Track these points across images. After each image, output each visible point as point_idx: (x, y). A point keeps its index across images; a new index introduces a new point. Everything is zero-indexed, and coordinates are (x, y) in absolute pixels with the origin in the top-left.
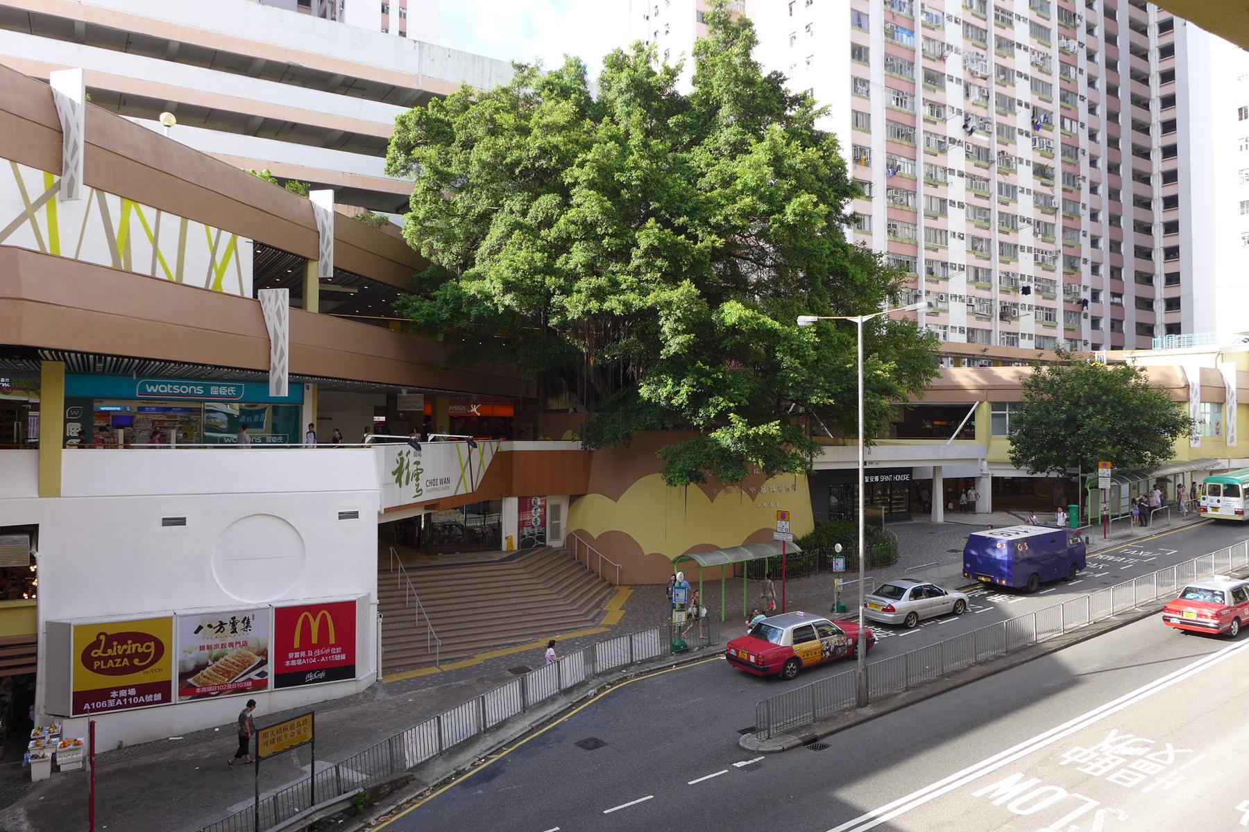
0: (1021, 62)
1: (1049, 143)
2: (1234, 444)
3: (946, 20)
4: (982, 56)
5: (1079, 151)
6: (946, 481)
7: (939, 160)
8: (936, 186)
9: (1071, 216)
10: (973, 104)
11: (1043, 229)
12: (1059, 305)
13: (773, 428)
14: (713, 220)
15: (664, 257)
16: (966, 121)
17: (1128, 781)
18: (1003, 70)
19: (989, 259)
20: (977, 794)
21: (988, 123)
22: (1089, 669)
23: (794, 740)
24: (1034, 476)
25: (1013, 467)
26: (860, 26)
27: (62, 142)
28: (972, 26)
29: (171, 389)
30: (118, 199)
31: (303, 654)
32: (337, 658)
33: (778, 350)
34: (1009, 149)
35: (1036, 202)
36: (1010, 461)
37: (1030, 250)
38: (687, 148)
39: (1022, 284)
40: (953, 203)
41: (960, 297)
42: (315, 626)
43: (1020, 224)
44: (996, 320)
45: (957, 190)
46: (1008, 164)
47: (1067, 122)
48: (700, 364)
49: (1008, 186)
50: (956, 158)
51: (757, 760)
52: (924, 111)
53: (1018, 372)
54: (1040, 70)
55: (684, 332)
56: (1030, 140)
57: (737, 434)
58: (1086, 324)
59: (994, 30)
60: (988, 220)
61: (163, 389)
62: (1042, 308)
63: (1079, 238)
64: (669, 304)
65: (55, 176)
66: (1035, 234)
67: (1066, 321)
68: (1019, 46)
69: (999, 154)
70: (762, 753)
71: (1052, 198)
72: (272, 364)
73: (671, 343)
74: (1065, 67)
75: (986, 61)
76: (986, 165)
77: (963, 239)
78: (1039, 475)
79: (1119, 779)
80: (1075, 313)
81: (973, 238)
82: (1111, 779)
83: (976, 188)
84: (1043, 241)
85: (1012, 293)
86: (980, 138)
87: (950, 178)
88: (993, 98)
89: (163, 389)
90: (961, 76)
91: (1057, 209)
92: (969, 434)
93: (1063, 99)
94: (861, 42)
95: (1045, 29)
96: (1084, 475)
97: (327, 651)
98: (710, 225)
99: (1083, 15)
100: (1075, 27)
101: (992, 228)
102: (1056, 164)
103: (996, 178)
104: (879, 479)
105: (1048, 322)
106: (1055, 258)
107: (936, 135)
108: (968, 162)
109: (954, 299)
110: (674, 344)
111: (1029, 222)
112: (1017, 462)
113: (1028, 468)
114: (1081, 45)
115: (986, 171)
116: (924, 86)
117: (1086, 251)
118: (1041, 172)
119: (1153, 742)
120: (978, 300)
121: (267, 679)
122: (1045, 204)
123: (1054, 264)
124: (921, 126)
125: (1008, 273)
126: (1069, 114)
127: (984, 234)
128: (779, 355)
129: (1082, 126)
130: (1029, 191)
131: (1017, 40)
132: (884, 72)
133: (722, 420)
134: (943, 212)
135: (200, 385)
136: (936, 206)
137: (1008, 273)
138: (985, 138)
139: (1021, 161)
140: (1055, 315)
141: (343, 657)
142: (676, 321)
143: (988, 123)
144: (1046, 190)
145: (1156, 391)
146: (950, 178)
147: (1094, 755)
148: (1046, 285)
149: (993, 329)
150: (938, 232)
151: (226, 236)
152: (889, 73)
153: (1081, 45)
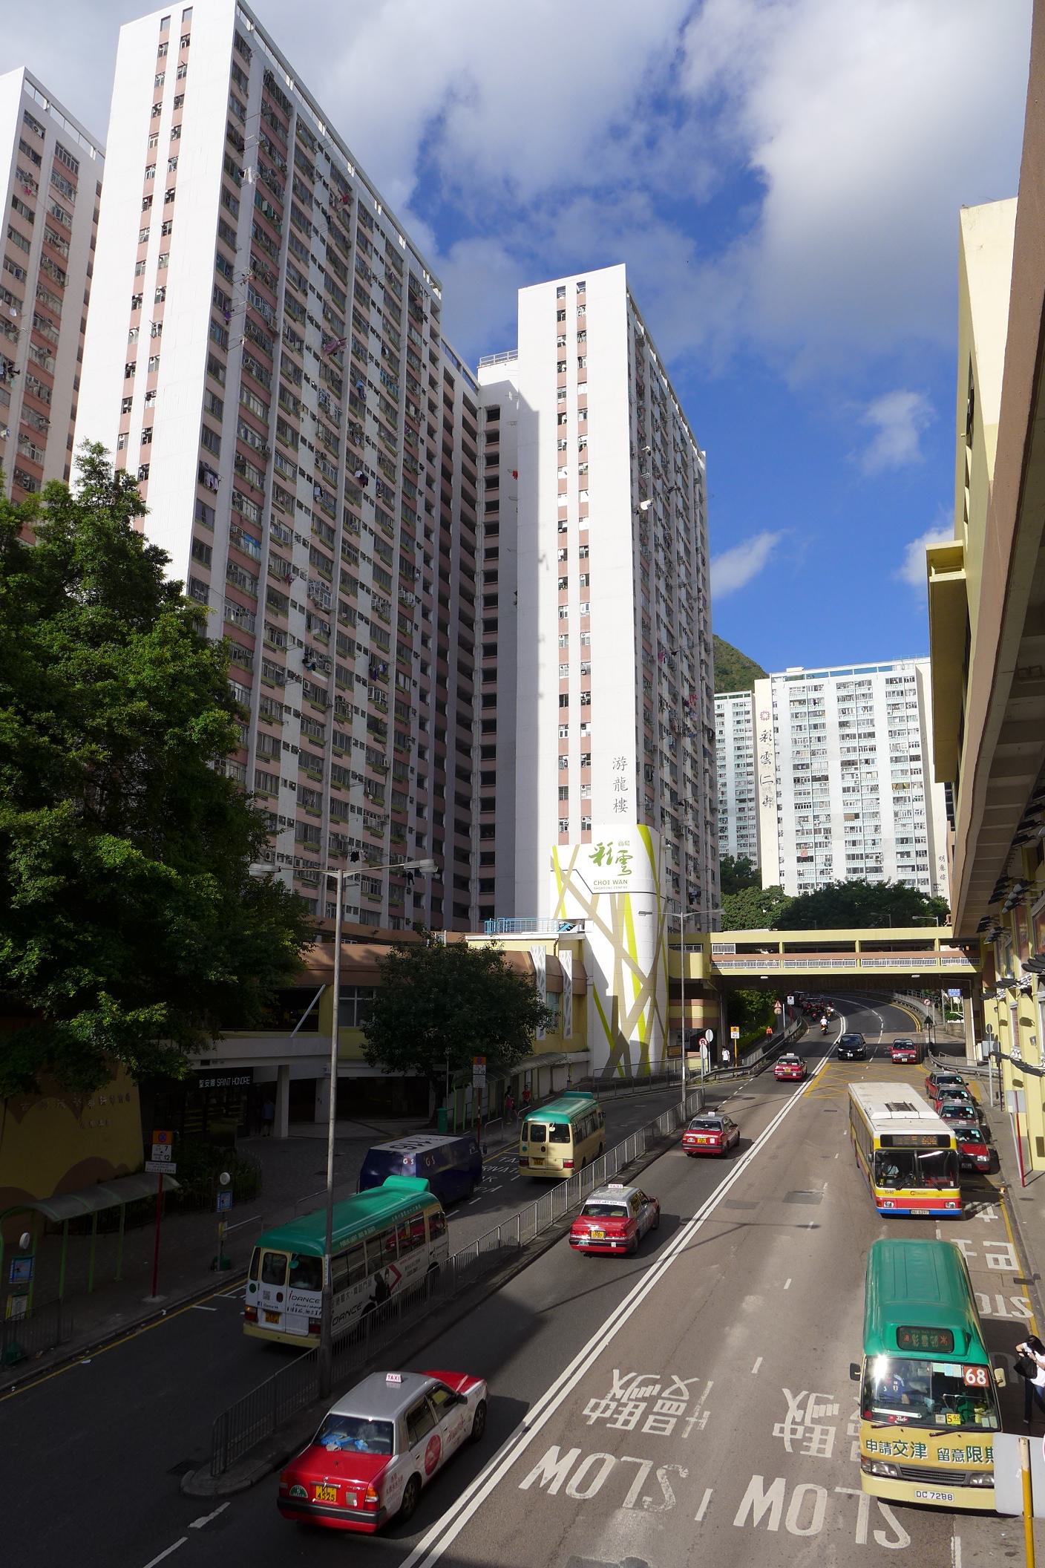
0: (363, 603)
1: (384, 696)
2: (571, 1036)
3: (294, 540)
4: (328, 588)
5: (411, 710)
6: (292, 1083)
7: (274, 694)
8: (270, 724)
9: (400, 779)
10: (315, 638)
11: (373, 790)
12: (385, 877)
13: (158, 1012)
14: (90, 723)
15: (15, 764)
16: (306, 655)
17: (664, 1429)
18: (345, 608)
19: (319, 816)
20: (525, 1485)
21: (328, 662)
22: (549, 1300)
23: (261, 1466)
24: (390, 1075)
25: (367, 1065)
26: (204, 520)
28: (319, 553)
33: (168, 907)
34: (346, 695)
35: (368, 758)
36: (364, 1058)
37: (360, 810)
38: (33, 620)
39: (352, 848)
40: (286, 746)
41: (288, 857)
43: (352, 781)
44: (323, 889)
45: (291, 732)
46: (344, 711)
47: (401, 677)
48: (59, 918)
49: (342, 735)
50: (293, 695)
51: (221, 1509)
52: (263, 635)
53: (368, 952)
54: (380, 617)
55: (48, 873)
56: (366, 689)
57: (107, 1021)
58: (409, 900)
59: (340, 564)
60: (320, 772)
62: (368, 878)
63: (406, 804)
64: (28, 830)
66: (366, 794)
67: (391, 895)
68: (363, 586)
69: (336, 697)
70: (224, 1497)
71: (384, 756)
73: (29, 885)
74: (403, 619)
75: (330, 594)
76: (323, 708)
77: (294, 789)
78: (396, 1074)
79: (652, 1428)
80: (399, 887)
81: (305, 788)
82: (646, 1429)
83: (311, 732)
84: (373, 802)
85: (340, 858)
86: (318, 677)
87: (286, 717)
88: (335, 636)
90: (304, 605)
91: (388, 769)
92: (312, 1025)
93: (399, 652)
94: (205, 539)
95: (387, 574)
96: (451, 1073)
98: (83, 729)
99: (421, 570)
100: (414, 580)
101: (324, 781)
102: (390, 720)
103: (332, 726)
104: (216, 1083)
105: (372, 896)
106: (383, 824)
107: (275, 664)
108: (306, 702)
109: (280, 859)
110: (33, 889)
111: (361, 780)
112: (370, 1059)
113: (384, 1066)
114: (418, 600)
115: (321, 714)
116: (267, 607)
117: (412, 821)
118: (375, 726)
119: (658, 1377)
120: (306, 863)
122: (376, 762)
123: (382, 830)
124: (261, 652)
125: (338, 835)
126: (404, 670)
127: (315, 786)
128: (169, 914)
129: (415, 684)
130: (362, 744)
131: (361, 579)
132: (226, 581)
133: (86, 1001)
134: (276, 756)
136: (268, 748)
137: (338, 835)
138: (323, 678)
139: (357, 709)
140: (380, 887)
142: (37, 857)
143: (328, 662)
144: (378, 747)
145: (520, 978)
146: (286, 717)
147: (613, 1405)
148: (373, 852)
149: (320, 899)
150: (269, 778)
152: (230, 583)
153: (418, 600)
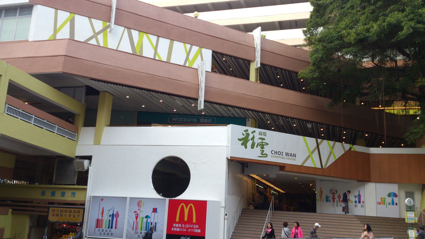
27: (255, 51)
29: (183, 119)
30: (138, 32)
31: (180, 225)
32: (196, 231)
42: (186, 211)
61: (179, 119)
65: (107, 23)
72: (199, 96)
89: (179, 119)
97: (192, 226)
121: (138, 216)
135: (195, 118)
141: (199, 231)
151: (195, 49)
